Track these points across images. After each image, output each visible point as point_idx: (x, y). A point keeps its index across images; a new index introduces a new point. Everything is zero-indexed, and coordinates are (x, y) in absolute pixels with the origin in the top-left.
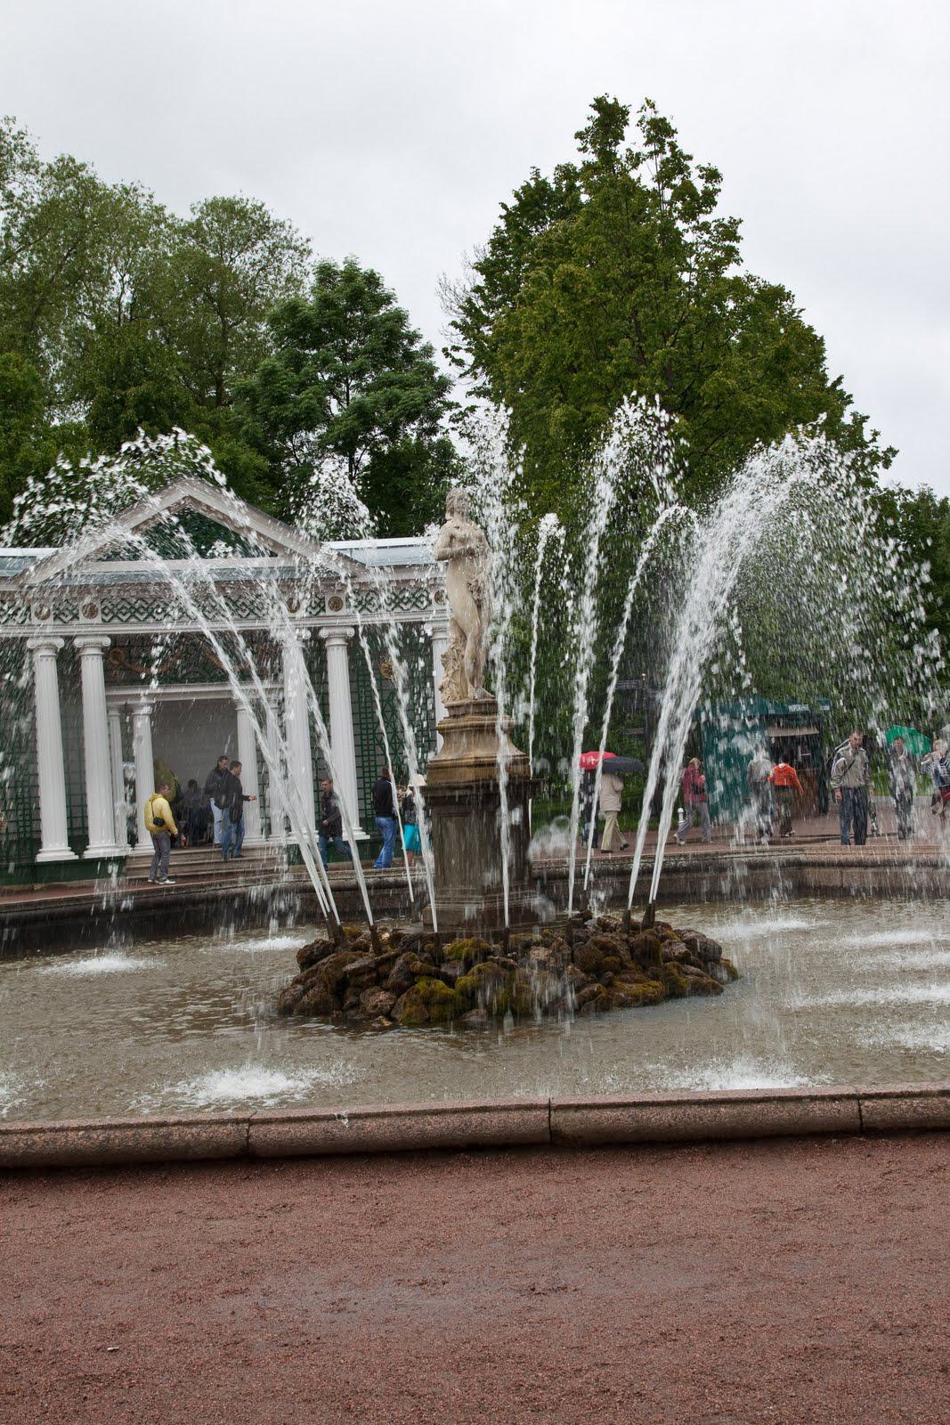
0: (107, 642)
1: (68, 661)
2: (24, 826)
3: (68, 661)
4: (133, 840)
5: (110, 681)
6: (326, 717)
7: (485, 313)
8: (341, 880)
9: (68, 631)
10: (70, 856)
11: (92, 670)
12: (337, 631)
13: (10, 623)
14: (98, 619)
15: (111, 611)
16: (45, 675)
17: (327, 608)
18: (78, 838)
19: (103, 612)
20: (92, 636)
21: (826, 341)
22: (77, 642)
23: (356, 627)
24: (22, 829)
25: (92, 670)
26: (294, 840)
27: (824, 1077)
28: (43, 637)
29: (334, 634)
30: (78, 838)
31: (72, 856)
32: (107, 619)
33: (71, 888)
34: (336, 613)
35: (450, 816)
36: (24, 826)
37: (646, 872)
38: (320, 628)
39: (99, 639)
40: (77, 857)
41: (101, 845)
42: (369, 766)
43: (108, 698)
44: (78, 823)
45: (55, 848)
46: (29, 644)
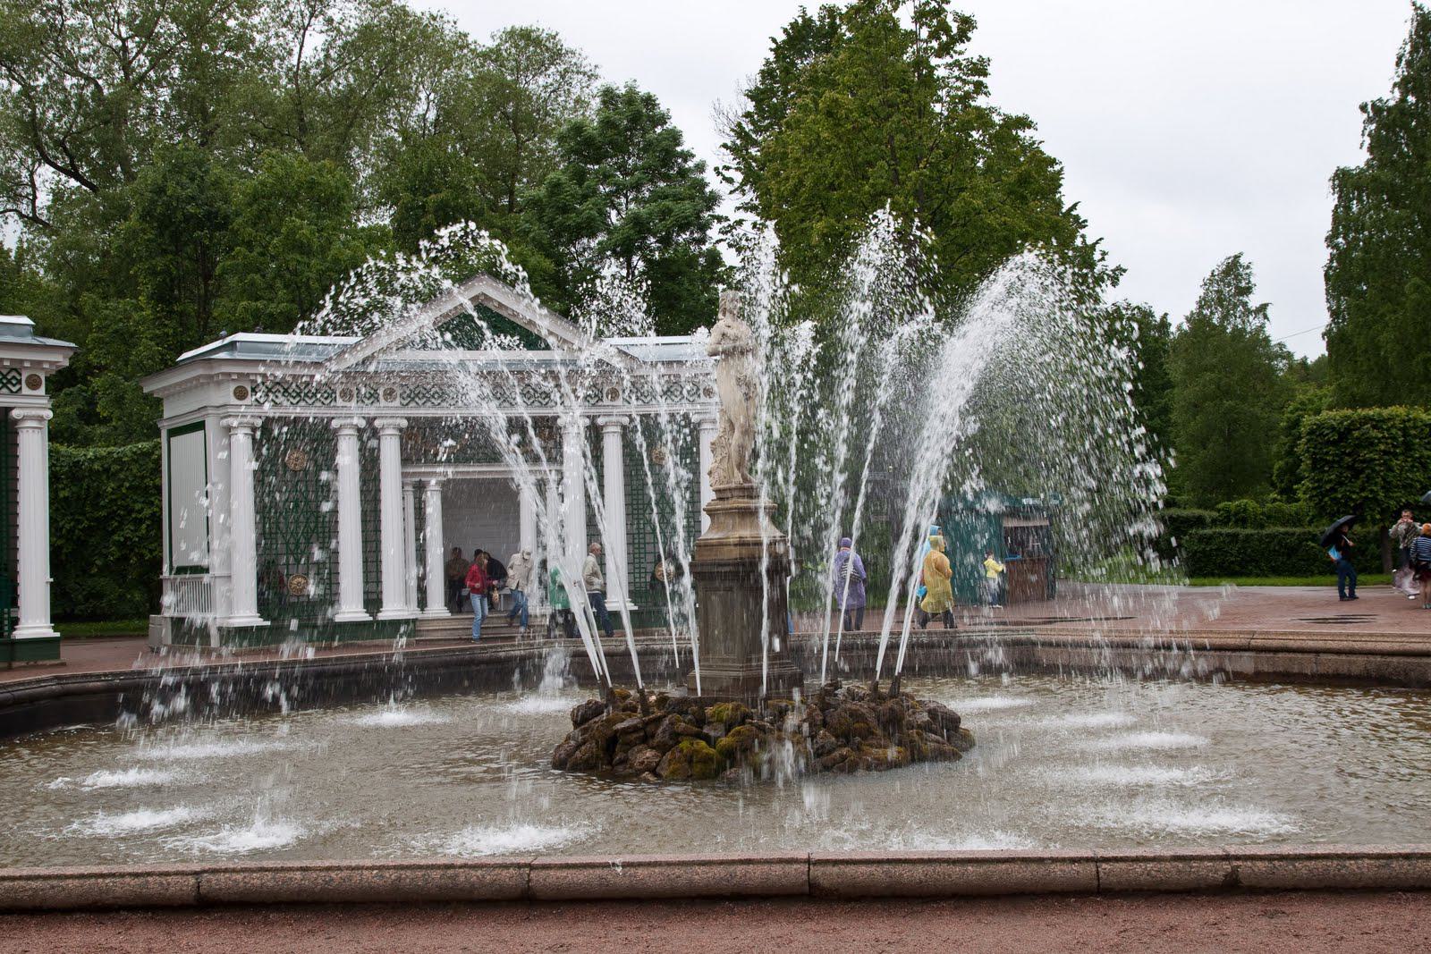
4: (422, 603)
5: (405, 461)
14: (397, 403)
18: (373, 601)
22: (600, 421)
30: (373, 601)
31: (367, 618)
37: (893, 647)
38: (12, 409)
41: (394, 607)
43: (404, 475)
45: (350, 609)
46: (335, 424)
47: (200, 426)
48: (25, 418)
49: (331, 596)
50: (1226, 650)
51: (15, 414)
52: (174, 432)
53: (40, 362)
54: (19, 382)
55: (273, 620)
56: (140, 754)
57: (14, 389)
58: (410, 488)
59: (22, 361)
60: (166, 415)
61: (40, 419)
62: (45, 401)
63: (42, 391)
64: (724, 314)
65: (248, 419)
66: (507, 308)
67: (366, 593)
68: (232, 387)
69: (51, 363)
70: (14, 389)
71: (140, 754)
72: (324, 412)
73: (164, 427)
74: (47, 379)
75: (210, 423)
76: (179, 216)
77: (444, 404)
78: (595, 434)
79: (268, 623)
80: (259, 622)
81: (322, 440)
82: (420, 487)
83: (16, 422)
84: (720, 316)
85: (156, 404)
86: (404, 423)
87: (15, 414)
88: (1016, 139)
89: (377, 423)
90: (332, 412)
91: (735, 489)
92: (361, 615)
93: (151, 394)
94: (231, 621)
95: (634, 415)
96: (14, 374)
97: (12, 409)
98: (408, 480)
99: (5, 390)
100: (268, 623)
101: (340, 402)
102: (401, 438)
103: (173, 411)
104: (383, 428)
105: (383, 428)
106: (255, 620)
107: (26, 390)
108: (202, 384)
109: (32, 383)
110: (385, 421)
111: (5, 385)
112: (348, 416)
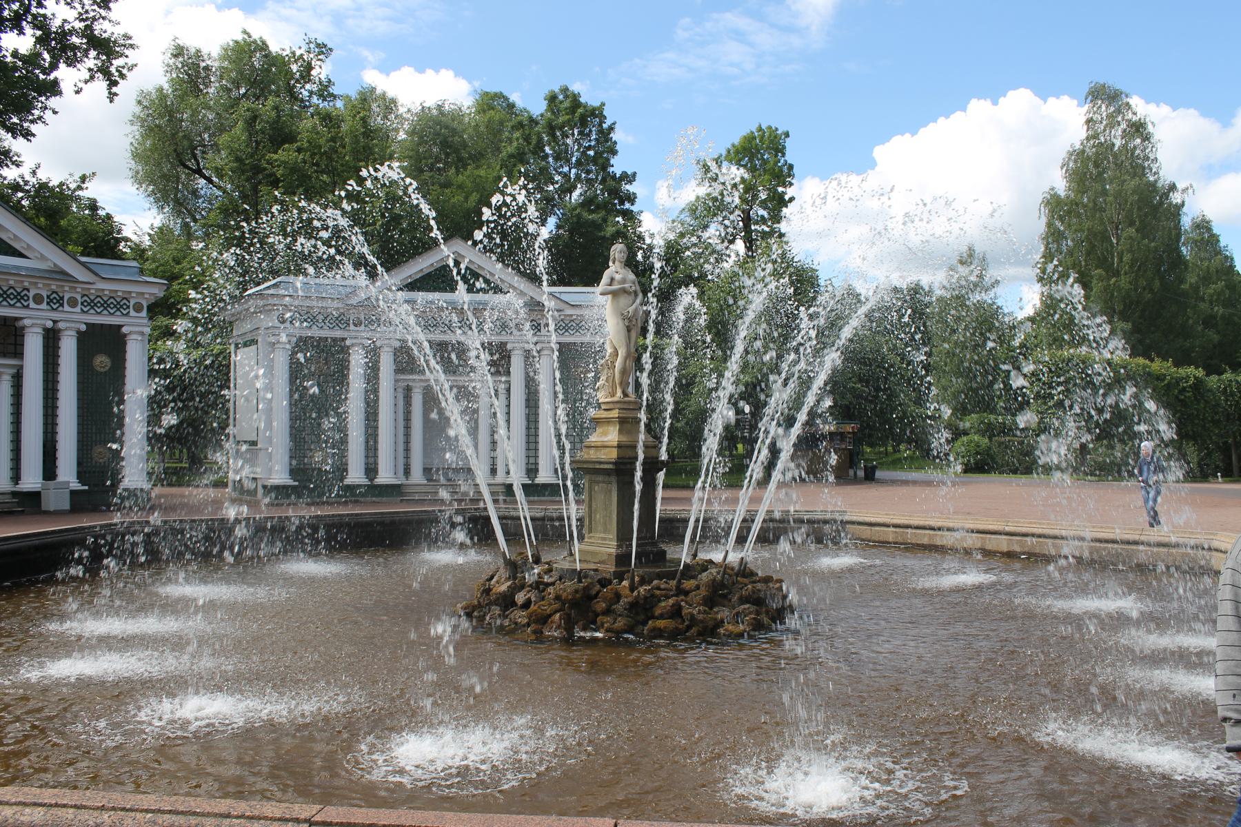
1: (51, 339)
3: (51, 339)
4: (407, 472)
5: (398, 371)
7: (1137, 223)
10: (365, 481)
12: (137, 329)
14: (78, 309)
16: (33, 346)
17: (351, 325)
18: (371, 470)
19: (82, 304)
20: (73, 321)
21: (386, 90)
22: (61, 325)
27: (786, 699)
28: (34, 321)
30: (371, 470)
32: (85, 309)
33: (364, 502)
35: (598, 482)
37: (525, 518)
38: (122, 326)
39: (77, 325)
43: (396, 381)
44: (532, 460)
45: (355, 476)
47: (254, 342)
48: (131, 333)
50: (1000, 534)
51: (124, 330)
53: (143, 294)
54: (128, 307)
56: (72, 627)
57: (125, 312)
58: (400, 390)
59: (130, 292)
61: (142, 334)
62: (146, 321)
63: (144, 313)
64: (614, 263)
66: (484, 269)
67: (366, 464)
69: (150, 294)
70: (125, 312)
71: (72, 627)
72: (338, 334)
74: (148, 307)
79: (86, 488)
80: (291, 482)
82: (408, 391)
83: (125, 335)
84: (611, 264)
86: (83, 328)
87: (125, 330)
90: (345, 334)
91: (617, 402)
95: (476, 331)
96: (125, 301)
97: (122, 326)
99: (5, 303)
101: (45, 294)
105: (66, 329)
106: (288, 481)
107: (133, 313)
109: (138, 308)
110: (131, 329)
111: (5, 299)
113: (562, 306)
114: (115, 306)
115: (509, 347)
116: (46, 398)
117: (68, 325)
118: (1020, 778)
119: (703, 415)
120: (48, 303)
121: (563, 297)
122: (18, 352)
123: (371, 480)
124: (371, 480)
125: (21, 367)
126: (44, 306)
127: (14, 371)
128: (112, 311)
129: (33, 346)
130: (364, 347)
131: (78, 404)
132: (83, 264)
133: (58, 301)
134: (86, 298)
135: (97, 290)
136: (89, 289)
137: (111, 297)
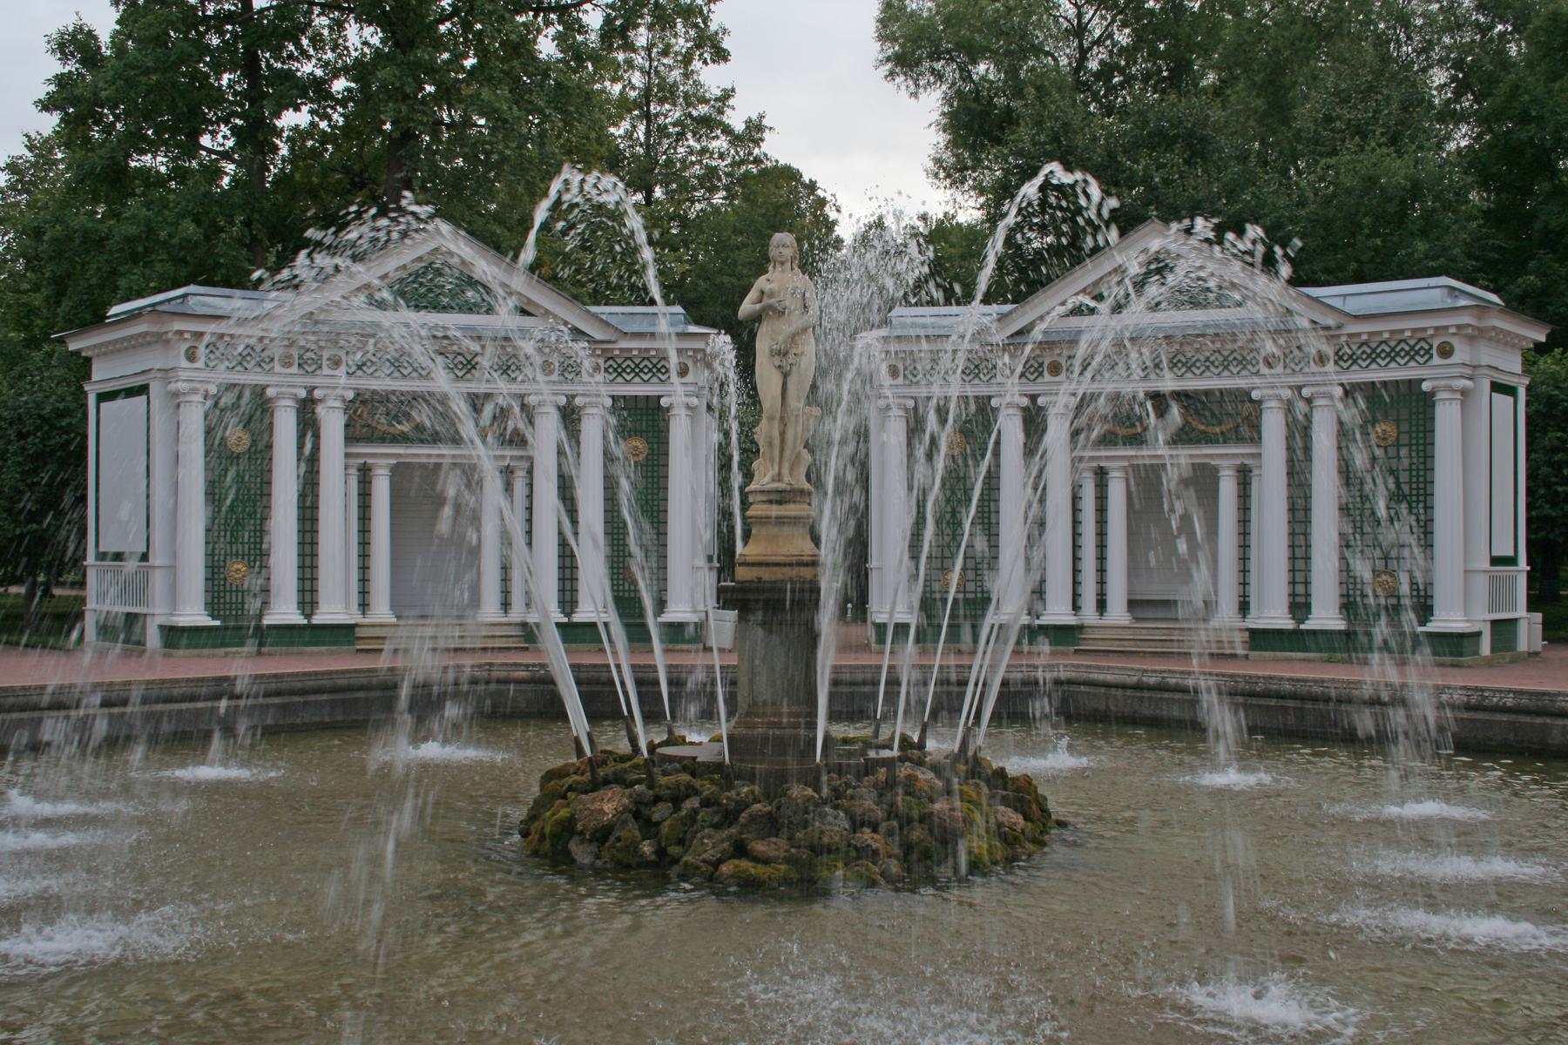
0: (350, 395)
2: (1418, 489)
4: (364, 606)
5: (351, 438)
6: (575, 523)
8: (642, 660)
9: (311, 381)
11: (332, 423)
12: (1442, 383)
13: (377, 374)
15: (615, 370)
17: (324, 366)
22: (578, 401)
23: (915, 399)
24: (1414, 492)
25: (332, 423)
26: (532, 618)
29: (282, 393)
31: (301, 620)
34: (333, 373)
36: (1418, 489)
38: (990, 398)
39: (294, 390)
40: (305, 622)
42: (1418, 482)
43: (347, 455)
46: (994, 402)
47: (143, 390)
49: (476, 602)
52: (104, 397)
55: (224, 618)
58: (353, 471)
60: (95, 377)
61: (1280, 399)
65: (339, 392)
67: (1293, 595)
68: (184, 347)
73: (91, 391)
75: (155, 388)
76: (974, 105)
77: (1244, 373)
78: (1034, 421)
79: (218, 623)
81: (262, 406)
85: (83, 366)
88: (117, 42)
89: (1040, 401)
92: (298, 619)
93: (77, 353)
94: (175, 619)
98: (352, 461)
100: (218, 623)
101: (326, 371)
102: (298, 412)
103: (103, 374)
104: (584, 407)
105: (584, 407)
108: (149, 343)
112: (284, 387)
113: (1342, 320)
114: (633, 370)
115: (270, 392)
116: (302, 532)
117: (588, 400)
118: (514, 883)
119: (730, 457)
120: (1336, 363)
121: (613, 321)
122: (1256, 439)
123: (308, 616)
124: (308, 616)
125: (530, 459)
126: (294, 369)
127: (525, 465)
128: (628, 378)
129: (1273, 426)
130: (1280, 399)
131: (1433, 450)
132: (595, 316)
133: (1036, 370)
134: (611, 362)
135: (621, 350)
136: (613, 350)
137: (626, 359)
